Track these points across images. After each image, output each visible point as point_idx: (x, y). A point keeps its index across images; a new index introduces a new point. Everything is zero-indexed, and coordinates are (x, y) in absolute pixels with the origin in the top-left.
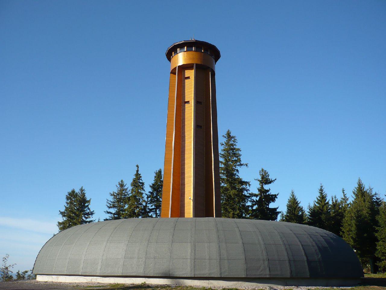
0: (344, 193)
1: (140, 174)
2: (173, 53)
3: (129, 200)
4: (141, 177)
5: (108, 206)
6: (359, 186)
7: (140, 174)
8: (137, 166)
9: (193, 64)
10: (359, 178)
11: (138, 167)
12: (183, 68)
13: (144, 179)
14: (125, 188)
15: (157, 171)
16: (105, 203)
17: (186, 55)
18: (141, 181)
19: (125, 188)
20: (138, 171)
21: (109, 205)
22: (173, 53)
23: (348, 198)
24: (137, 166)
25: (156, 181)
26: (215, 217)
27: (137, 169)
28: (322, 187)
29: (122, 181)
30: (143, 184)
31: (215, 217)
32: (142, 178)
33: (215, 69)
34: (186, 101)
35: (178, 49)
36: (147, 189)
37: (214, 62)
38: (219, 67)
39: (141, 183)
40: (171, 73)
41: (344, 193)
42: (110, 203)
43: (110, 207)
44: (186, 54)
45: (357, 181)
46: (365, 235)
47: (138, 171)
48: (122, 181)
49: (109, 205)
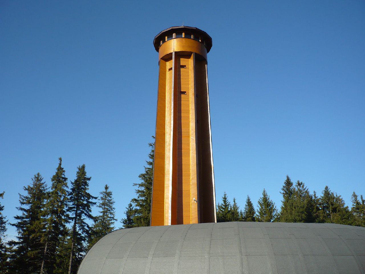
0: (234, 201)
1: (63, 168)
2: (166, 37)
3: (49, 197)
4: (64, 171)
5: (21, 202)
6: (264, 196)
7: (63, 168)
8: (61, 159)
9: (192, 53)
10: (264, 189)
11: (61, 160)
12: (179, 55)
13: (66, 175)
14: (42, 182)
15: (80, 166)
16: (18, 198)
17: (184, 42)
18: (63, 176)
19: (42, 182)
20: (60, 164)
21: (22, 201)
22: (166, 37)
23: (238, 207)
24: (61, 159)
25: (79, 177)
26: (216, 222)
27: (59, 163)
28: (225, 195)
29: (38, 174)
30: (66, 179)
31: (216, 222)
32: (65, 174)
33: (207, 57)
34: (182, 91)
35: (174, 35)
36: (69, 187)
37: (206, 51)
38: (210, 56)
39: (63, 178)
40: (161, 59)
41: (234, 201)
42: (23, 198)
43: (22, 203)
44: (184, 40)
45: (262, 192)
46: (29, 249)
47: (60, 164)
48: (38, 174)
49: (22, 201)
